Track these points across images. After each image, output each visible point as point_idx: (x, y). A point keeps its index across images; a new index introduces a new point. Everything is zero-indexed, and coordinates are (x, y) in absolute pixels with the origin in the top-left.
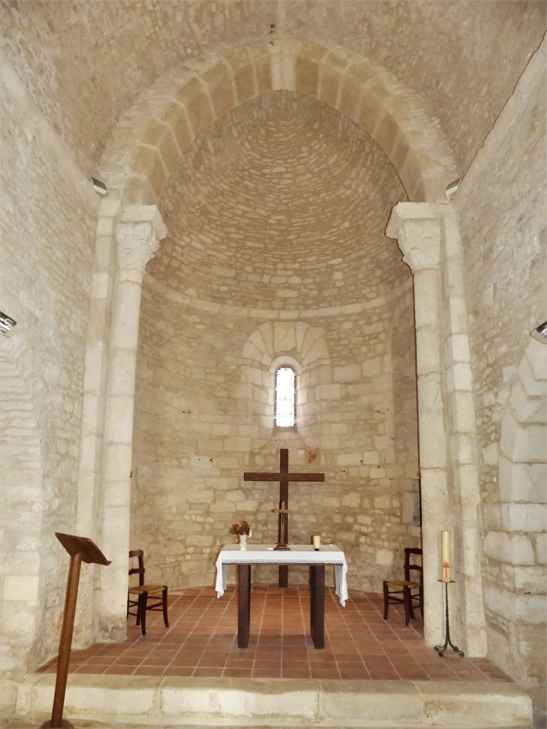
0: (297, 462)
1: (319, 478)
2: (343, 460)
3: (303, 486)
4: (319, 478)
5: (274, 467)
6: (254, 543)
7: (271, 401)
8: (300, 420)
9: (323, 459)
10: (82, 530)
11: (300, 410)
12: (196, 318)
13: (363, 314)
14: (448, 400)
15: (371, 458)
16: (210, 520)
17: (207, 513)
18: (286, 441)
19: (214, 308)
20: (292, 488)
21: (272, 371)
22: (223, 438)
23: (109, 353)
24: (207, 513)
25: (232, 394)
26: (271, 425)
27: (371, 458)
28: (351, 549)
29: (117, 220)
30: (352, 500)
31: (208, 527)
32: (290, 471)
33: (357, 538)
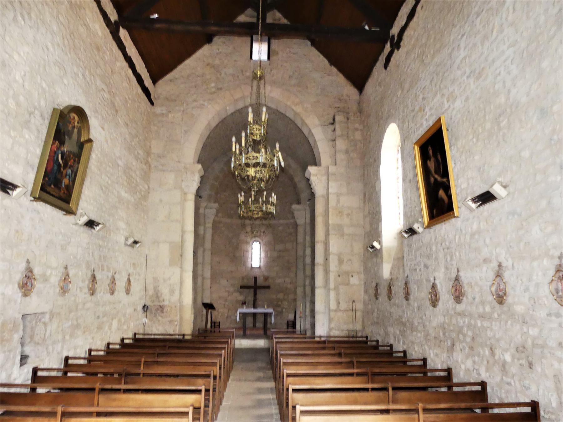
0: (260, 282)
1: (268, 287)
2: (278, 281)
3: (263, 291)
4: (268, 287)
5: (252, 283)
6: (247, 307)
7: (250, 256)
8: (262, 264)
9: (270, 280)
10: (207, 301)
11: (262, 260)
12: (222, 225)
13: (287, 224)
14: (304, 265)
15: (288, 280)
16: (227, 303)
17: (226, 300)
18: (257, 273)
19: (228, 221)
20: (258, 291)
21: (251, 243)
22: (232, 272)
23: (204, 251)
24: (226, 300)
25: (237, 255)
26: (250, 266)
27: (288, 280)
28: (275, 307)
29: (206, 207)
30: (281, 296)
31: (226, 306)
32: (428, 368)
33: (282, 310)
